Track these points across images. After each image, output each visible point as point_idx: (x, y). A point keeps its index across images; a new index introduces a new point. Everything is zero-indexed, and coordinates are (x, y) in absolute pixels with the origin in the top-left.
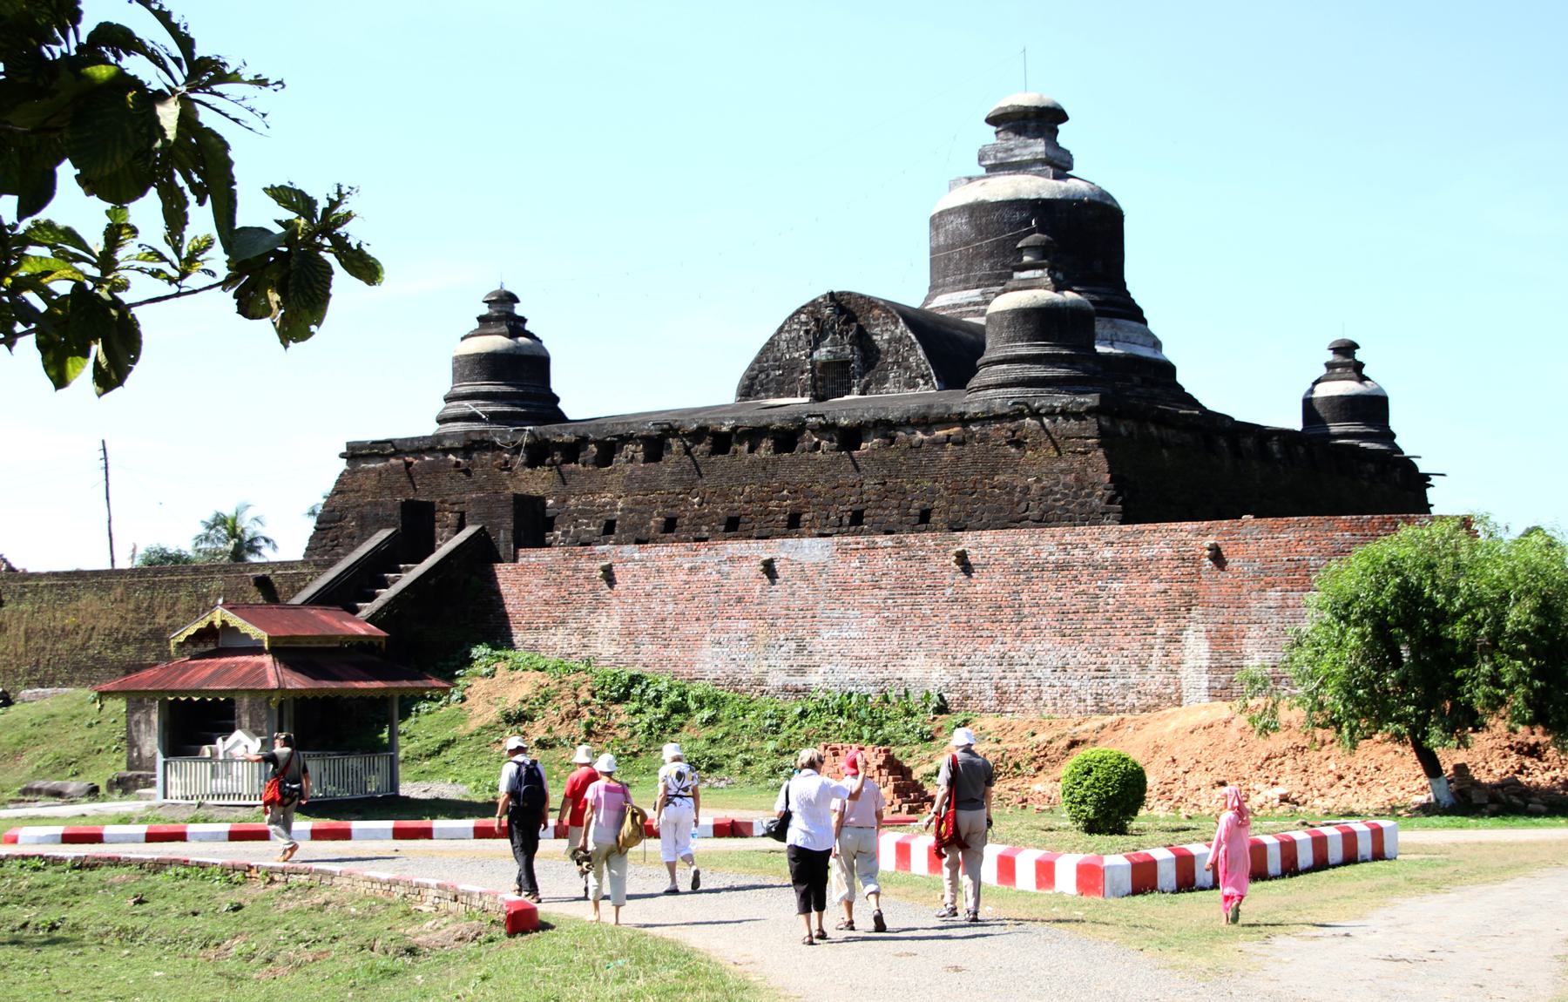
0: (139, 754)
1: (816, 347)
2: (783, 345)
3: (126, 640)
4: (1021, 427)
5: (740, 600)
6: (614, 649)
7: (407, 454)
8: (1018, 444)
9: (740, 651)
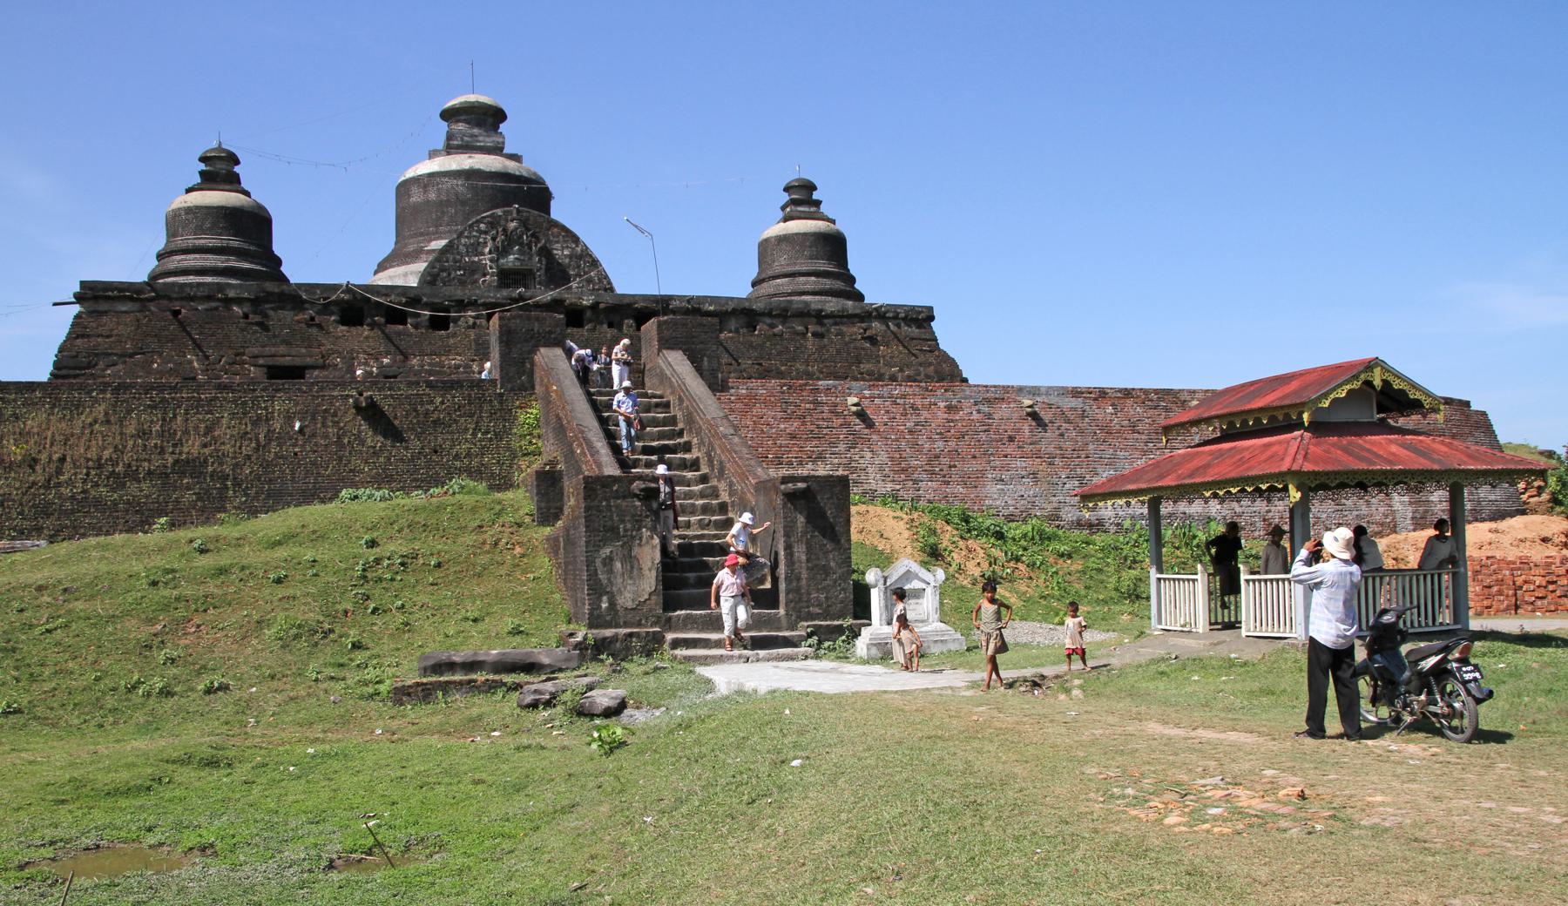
0: (612, 604)
3: (132, 474)
5: (1011, 439)
9: (1027, 489)
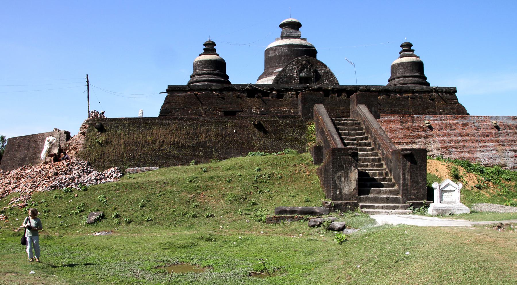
0: (341, 192)
1: (301, 72)
2: (287, 71)
4: (432, 95)
5: (487, 136)
6: (440, 153)
7: (195, 91)
8: (433, 100)
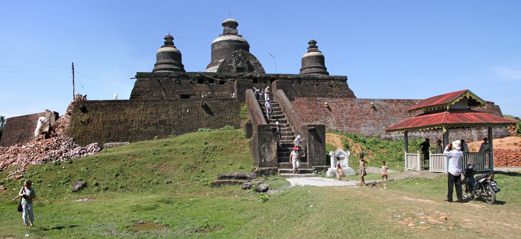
0: (265, 161)
